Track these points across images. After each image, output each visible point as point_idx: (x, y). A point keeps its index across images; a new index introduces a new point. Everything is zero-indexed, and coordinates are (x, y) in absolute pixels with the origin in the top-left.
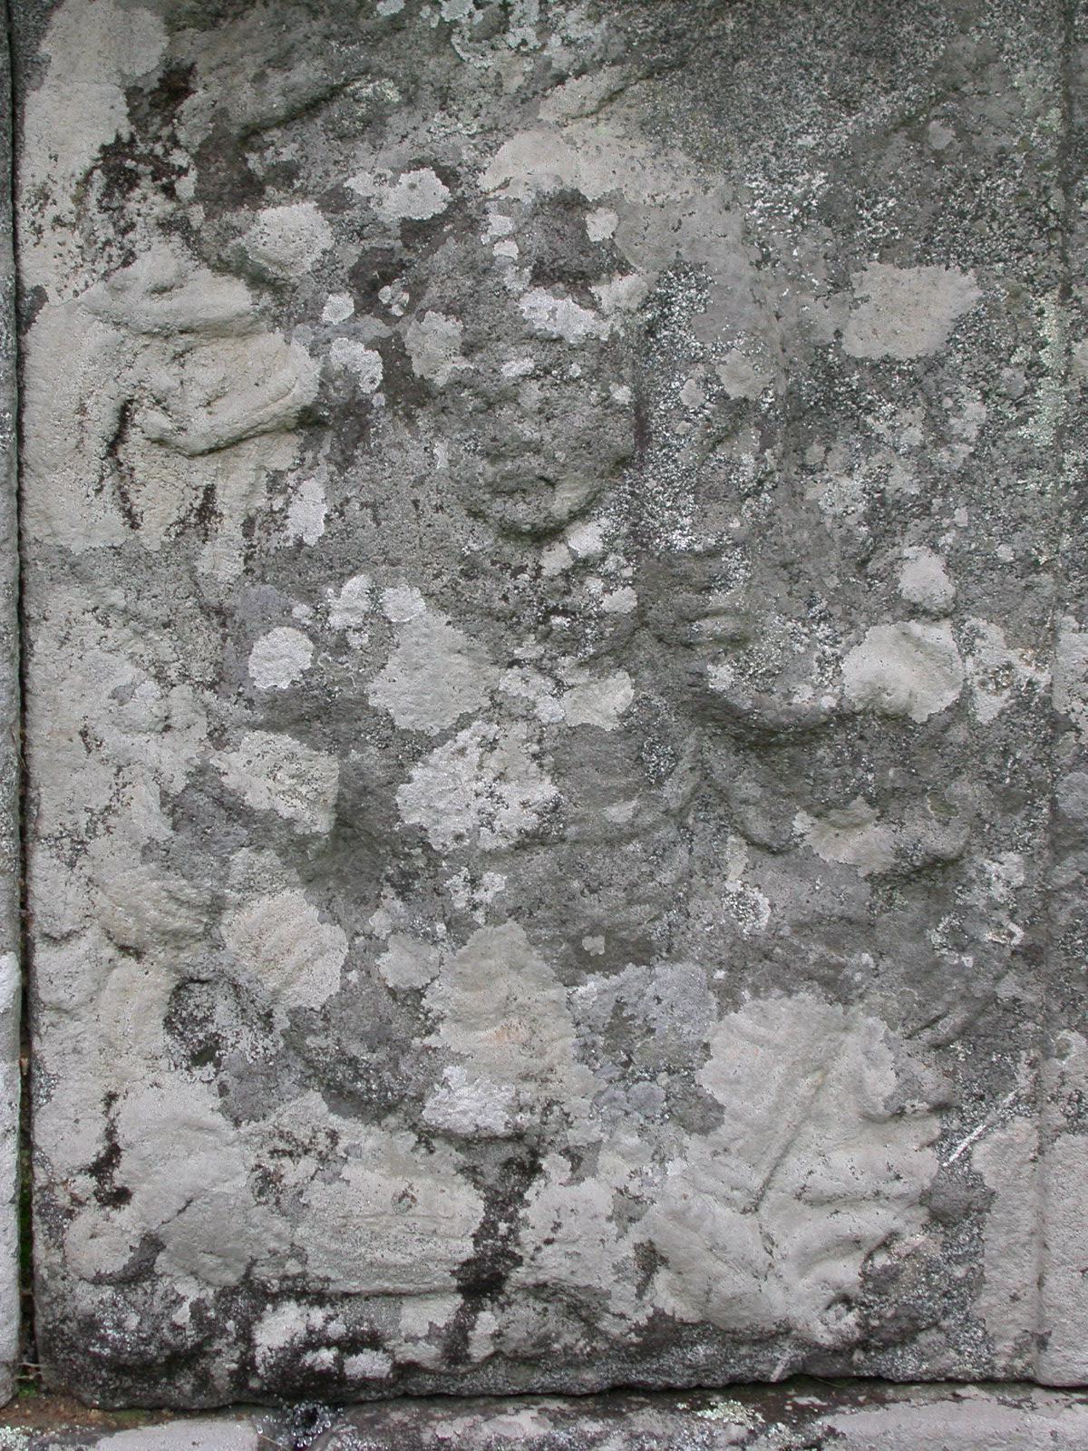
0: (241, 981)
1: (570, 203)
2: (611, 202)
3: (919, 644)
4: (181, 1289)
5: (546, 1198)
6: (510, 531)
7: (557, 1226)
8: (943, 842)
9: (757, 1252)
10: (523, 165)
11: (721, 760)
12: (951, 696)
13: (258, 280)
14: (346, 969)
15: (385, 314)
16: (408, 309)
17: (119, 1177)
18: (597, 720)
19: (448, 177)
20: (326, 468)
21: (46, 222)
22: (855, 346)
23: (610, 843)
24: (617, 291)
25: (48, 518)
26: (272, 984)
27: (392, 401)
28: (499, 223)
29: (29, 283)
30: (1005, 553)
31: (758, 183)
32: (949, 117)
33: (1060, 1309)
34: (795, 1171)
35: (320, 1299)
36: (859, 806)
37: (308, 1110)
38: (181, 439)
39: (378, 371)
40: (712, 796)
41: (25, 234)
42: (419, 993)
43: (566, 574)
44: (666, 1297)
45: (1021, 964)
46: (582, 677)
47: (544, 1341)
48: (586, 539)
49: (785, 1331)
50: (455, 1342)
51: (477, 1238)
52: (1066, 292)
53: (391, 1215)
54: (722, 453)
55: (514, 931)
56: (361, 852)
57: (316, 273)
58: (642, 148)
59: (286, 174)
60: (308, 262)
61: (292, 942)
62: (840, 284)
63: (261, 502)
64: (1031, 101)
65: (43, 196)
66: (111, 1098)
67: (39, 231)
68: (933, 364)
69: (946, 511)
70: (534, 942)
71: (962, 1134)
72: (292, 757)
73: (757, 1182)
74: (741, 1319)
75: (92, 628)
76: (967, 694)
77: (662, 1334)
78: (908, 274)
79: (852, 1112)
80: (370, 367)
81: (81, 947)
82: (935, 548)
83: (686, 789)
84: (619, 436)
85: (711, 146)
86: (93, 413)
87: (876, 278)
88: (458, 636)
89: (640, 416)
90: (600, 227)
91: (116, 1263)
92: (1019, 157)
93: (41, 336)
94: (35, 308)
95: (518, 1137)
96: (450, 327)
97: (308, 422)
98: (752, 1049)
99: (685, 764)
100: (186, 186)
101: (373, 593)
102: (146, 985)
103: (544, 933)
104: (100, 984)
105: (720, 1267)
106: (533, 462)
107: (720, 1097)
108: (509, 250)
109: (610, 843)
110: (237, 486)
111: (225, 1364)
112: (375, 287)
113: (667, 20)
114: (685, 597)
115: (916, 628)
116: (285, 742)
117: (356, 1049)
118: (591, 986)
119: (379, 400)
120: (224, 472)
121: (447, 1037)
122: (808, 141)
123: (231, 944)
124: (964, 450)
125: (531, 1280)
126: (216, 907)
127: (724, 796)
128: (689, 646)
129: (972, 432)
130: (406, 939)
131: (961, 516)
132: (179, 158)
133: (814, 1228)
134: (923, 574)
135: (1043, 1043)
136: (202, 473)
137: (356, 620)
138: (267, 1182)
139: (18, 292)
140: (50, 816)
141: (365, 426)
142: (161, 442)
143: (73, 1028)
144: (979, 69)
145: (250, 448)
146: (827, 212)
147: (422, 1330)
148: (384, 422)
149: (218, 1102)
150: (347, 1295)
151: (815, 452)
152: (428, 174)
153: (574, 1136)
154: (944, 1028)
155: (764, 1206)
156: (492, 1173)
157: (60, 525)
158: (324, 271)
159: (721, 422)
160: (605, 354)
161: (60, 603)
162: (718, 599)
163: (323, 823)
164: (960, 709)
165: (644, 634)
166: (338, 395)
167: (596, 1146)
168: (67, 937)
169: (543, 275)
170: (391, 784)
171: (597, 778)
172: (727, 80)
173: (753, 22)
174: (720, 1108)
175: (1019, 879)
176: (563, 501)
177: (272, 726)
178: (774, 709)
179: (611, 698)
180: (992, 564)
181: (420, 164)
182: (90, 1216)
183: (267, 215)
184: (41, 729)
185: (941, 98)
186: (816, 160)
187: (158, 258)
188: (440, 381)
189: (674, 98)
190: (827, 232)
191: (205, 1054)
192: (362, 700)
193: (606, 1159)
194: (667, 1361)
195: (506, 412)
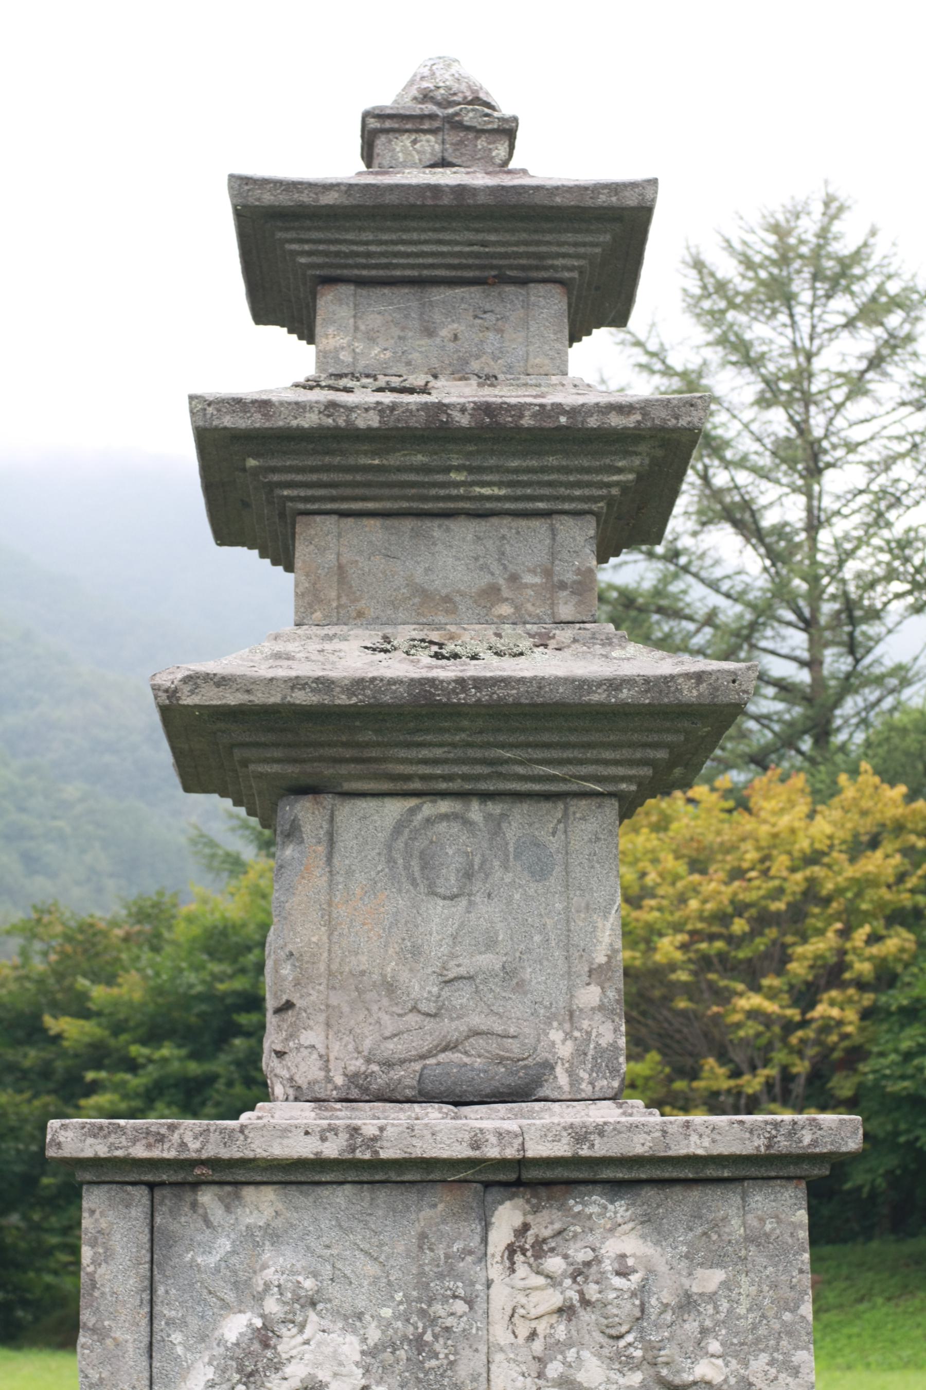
1: (623, 1256)
2: (634, 1255)
6: (612, 1337)
10: (612, 1247)
12: (723, 1378)
13: (548, 1276)
16: (584, 1282)
19: (593, 1250)
22: (695, 1289)
24: (635, 1278)
28: (608, 1262)
30: (735, 1341)
31: (669, 1249)
48: (630, 1338)
59: (552, 1250)
60: (560, 1272)
62: (690, 1274)
64: (736, 1227)
65: (493, 1255)
68: (715, 1293)
75: (505, 1364)
76: (727, 1377)
80: (576, 1297)
84: (638, 1314)
87: (699, 1272)
88: (599, 1363)
90: (630, 1262)
97: (560, 1311)
101: (578, 1353)
108: (610, 1268)
110: (542, 1327)
115: (713, 1360)
119: (578, 1305)
124: (723, 1315)
132: (527, 1246)
134: (714, 1346)
136: (534, 1324)
144: (723, 1220)
145: (545, 1318)
146: (687, 1257)
148: (581, 1312)
151: (686, 1317)
158: (564, 1275)
160: (634, 1294)
161: (498, 1357)
162: (662, 1353)
164: (726, 1380)
169: (618, 1274)
172: (661, 1224)
176: (624, 1329)
180: (732, 1344)
186: (683, 1243)
187: (522, 1270)
189: (647, 1229)
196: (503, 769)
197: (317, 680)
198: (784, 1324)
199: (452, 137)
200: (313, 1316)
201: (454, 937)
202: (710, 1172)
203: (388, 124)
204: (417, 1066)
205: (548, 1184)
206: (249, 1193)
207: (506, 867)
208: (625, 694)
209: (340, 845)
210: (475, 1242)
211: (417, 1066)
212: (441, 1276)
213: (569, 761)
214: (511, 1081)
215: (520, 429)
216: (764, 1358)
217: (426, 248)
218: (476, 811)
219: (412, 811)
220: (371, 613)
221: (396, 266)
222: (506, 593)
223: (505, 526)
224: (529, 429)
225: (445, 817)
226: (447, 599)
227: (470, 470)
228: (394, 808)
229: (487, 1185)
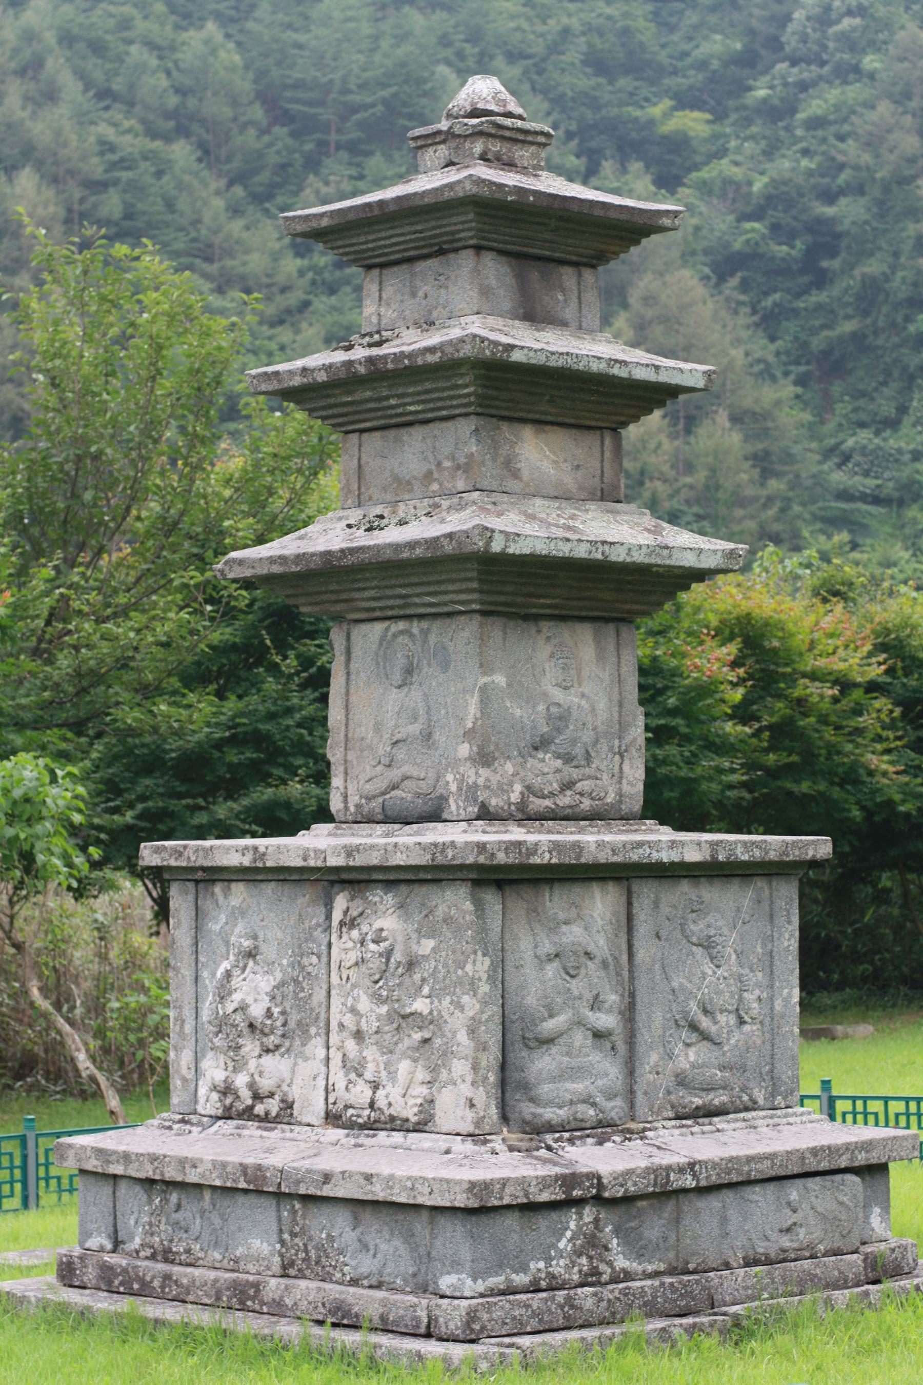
44: (392, 1111)
138: (347, 1088)
160: (381, 955)
169: (374, 941)
196: (409, 601)
197: (280, 557)
198: (458, 977)
199: (453, 144)
200: (251, 963)
201: (398, 713)
202: (422, 876)
203: (420, 143)
204: (380, 800)
205: (359, 882)
206: (234, 886)
207: (429, 665)
208: (418, 551)
209: (353, 655)
210: (322, 919)
211: (380, 800)
212: (306, 940)
213: (441, 593)
214: (427, 808)
215: (388, 371)
216: (448, 999)
217: (394, 240)
218: (416, 627)
219: (387, 629)
220: (375, 497)
221: (386, 254)
222: (436, 476)
223: (436, 428)
224: (393, 370)
225: (401, 632)
226: (409, 483)
227: (399, 396)
228: (378, 628)
229: (332, 883)
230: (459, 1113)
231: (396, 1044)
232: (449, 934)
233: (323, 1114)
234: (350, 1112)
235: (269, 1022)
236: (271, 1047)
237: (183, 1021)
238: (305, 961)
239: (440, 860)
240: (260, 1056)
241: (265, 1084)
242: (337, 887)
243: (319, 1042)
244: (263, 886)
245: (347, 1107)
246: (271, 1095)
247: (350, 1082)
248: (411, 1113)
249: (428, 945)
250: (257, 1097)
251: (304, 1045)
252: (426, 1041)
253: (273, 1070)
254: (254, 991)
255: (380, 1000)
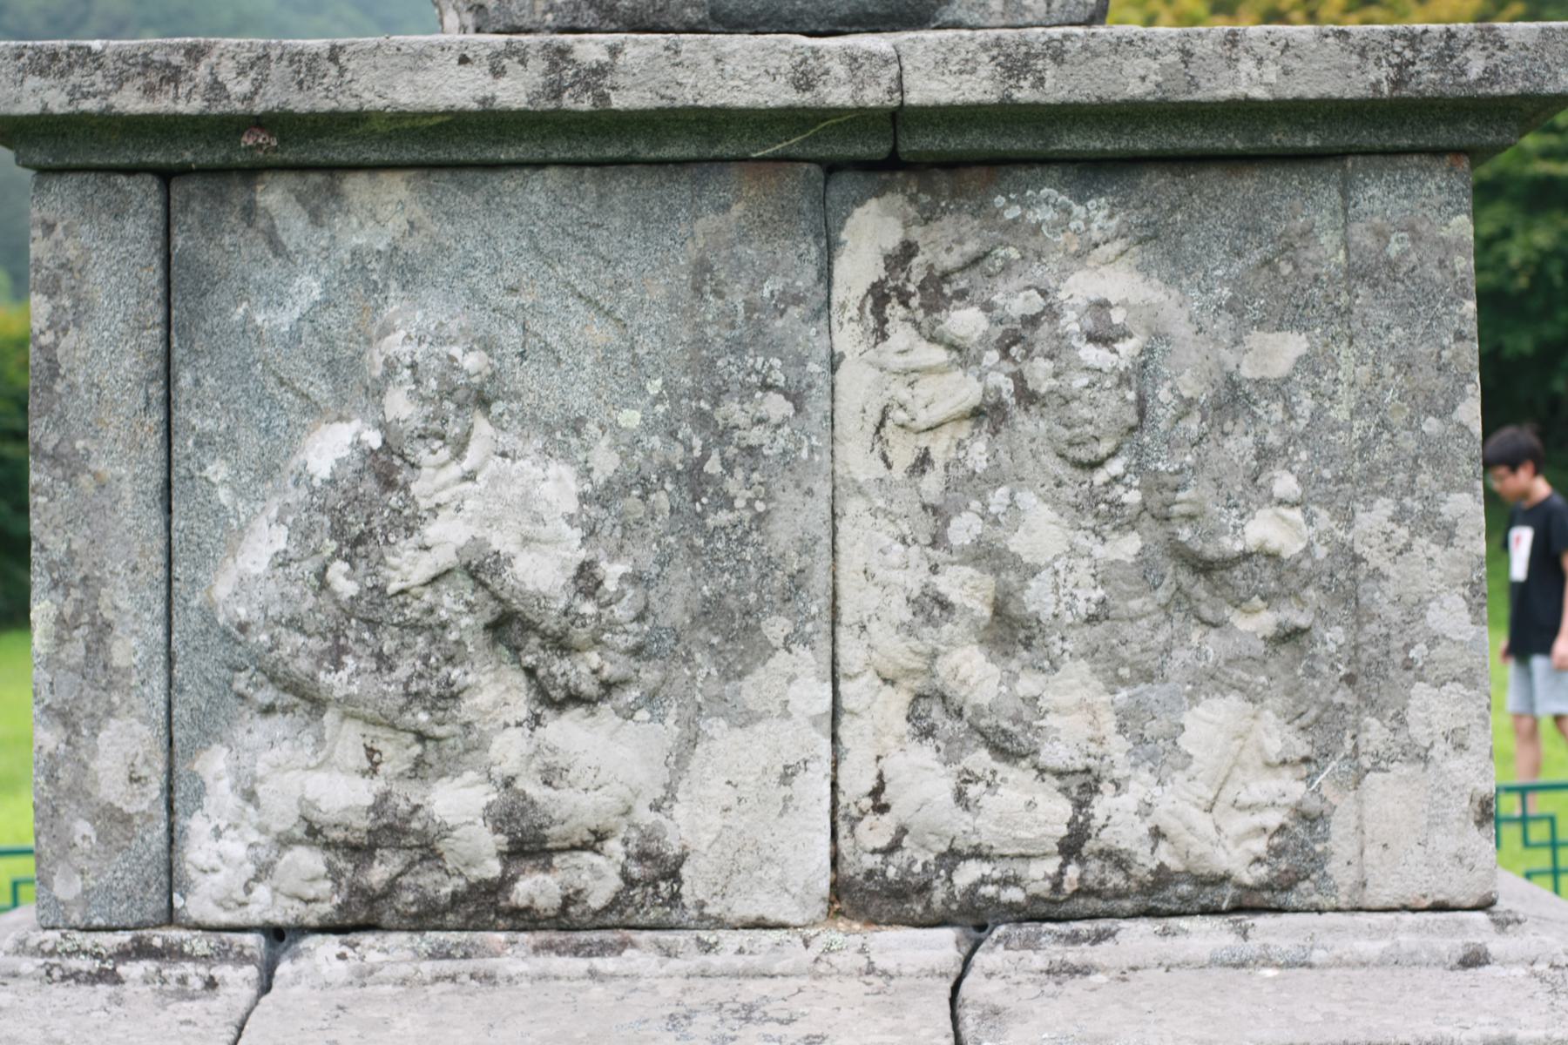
0: (947, 693)
1: (1103, 305)
2: (1124, 304)
3: (1284, 519)
4: (916, 855)
5: (1101, 806)
7: (1109, 818)
8: (1302, 621)
9: (1211, 831)
10: (1081, 288)
11: (1185, 578)
12: (1302, 546)
13: (951, 346)
14: (1000, 683)
15: (1014, 361)
16: (1025, 357)
17: (884, 799)
18: (1122, 557)
19: (1044, 293)
20: (986, 436)
21: (845, 320)
23: (1131, 620)
24: (1128, 349)
25: (847, 464)
26: (963, 693)
27: (1018, 403)
28: (1071, 315)
29: (837, 350)
30: (1327, 474)
31: (1196, 293)
32: (1289, 259)
33: (1373, 867)
34: (1229, 794)
35: (987, 858)
36: (1256, 601)
37: (980, 759)
38: (913, 424)
39: (1011, 386)
40: (1181, 596)
41: (835, 326)
42: (1037, 699)
43: (1106, 484)
44: (1165, 855)
45: (1344, 684)
46: (1115, 536)
47: (1102, 882)
48: (1116, 467)
49: (1224, 879)
50: (1057, 883)
51: (1069, 825)
52: (1351, 343)
53: (1025, 812)
54: (1181, 424)
55: (1084, 666)
56: (1009, 630)
57: (980, 342)
58: (1138, 278)
59: (961, 295)
60: (975, 337)
61: (975, 673)
62: (1237, 342)
63: (952, 455)
64: (1330, 249)
65: (843, 306)
66: (879, 758)
67: (841, 324)
68: (1287, 380)
69: (1296, 453)
70: (1094, 671)
71: (1317, 774)
72: (972, 578)
73: (1211, 796)
74: (1203, 869)
76: (1310, 545)
77: (1163, 877)
78: (1271, 337)
79: (1259, 762)
80: (1008, 386)
81: (863, 680)
82: (1291, 471)
83: (1169, 594)
84: (1133, 420)
85: (1172, 276)
86: (869, 412)
87: (1256, 338)
88: (1054, 516)
89: (1141, 402)
90: (1117, 316)
91: (883, 843)
92: (1325, 278)
93: (842, 375)
94: (839, 362)
95: (1088, 770)
96: (1048, 365)
97: (976, 414)
98: (1209, 724)
99: (1166, 581)
100: (914, 302)
102: (896, 702)
103: (1099, 666)
104: (874, 699)
105: (1192, 839)
106: (1090, 429)
107: (1190, 751)
108: (1076, 327)
109: (1131, 620)
110: (940, 448)
111: (939, 895)
112: (1008, 347)
113: (1147, 216)
114: (1167, 494)
115: (1283, 511)
116: (968, 571)
117: (1005, 724)
118: (1123, 694)
119: (1012, 401)
120: (934, 440)
121: (1051, 721)
122: (1219, 272)
123: (942, 674)
124: (1303, 422)
125: (1096, 848)
126: (934, 655)
127: (1188, 596)
128: (1168, 519)
129: (1307, 414)
130: (1028, 671)
131: (1304, 455)
132: (911, 288)
133: (1241, 823)
134: (1285, 484)
135: (1356, 725)
136: (924, 440)
137: (1003, 509)
138: (960, 796)
139: (832, 355)
140: (847, 614)
141: (1005, 414)
142: (902, 426)
143: (858, 722)
145: (948, 428)
146: (1230, 308)
147: (1041, 875)
149: (935, 755)
150: (1002, 856)
151: (1228, 426)
152: (1033, 292)
153: (1116, 773)
154: (1305, 721)
155: (1215, 809)
156: (1074, 791)
157: (852, 468)
158: (984, 343)
159: (1181, 408)
160: (1123, 380)
161: (853, 506)
162: (1181, 495)
163: (987, 613)
164: (1307, 551)
165: (1145, 515)
166: (991, 401)
167: (1128, 778)
168: (856, 676)
169: (1093, 338)
170: (1022, 589)
171: (1125, 587)
172: (1178, 244)
173: (1190, 216)
174: (1190, 756)
175: (1342, 641)
176: (1104, 448)
177: (962, 563)
178: (1211, 552)
179: (1128, 546)
180: (1321, 479)
181: (1029, 288)
182: (870, 819)
183: (954, 314)
184: (844, 570)
185: (1284, 251)
186: (1223, 281)
187: (901, 334)
188: (1043, 390)
190: (1230, 317)
191: (928, 733)
192: (1006, 548)
193: (1132, 785)
194: (1167, 894)
195: (1075, 404)
200: (482, 427)
202: (1278, 138)
206: (356, 186)
210: (806, 279)
216: (1385, 506)
230: (1445, 843)
231: (1167, 651)
232: (1386, 316)
233: (824, 886)
234: (968, 873)
235: (589, 608)
236: (588, 687)
237: (102, 631)
238: (733, 410)
239: (1427, 79)
240: (537, 720)
241: (572, 807)
242: (847, 182)
243: (808, 663)
244: (507, 183)
245: (952, 857)
246: (596, 840)
247: (968, 778)
248: (1238, 856)
249: (1279, 352)
250: (528, 845)
251: (730, 674)
252: (1290, 636)
253: (602, 763)
254: (512, 507)
255: (1107, 516)
